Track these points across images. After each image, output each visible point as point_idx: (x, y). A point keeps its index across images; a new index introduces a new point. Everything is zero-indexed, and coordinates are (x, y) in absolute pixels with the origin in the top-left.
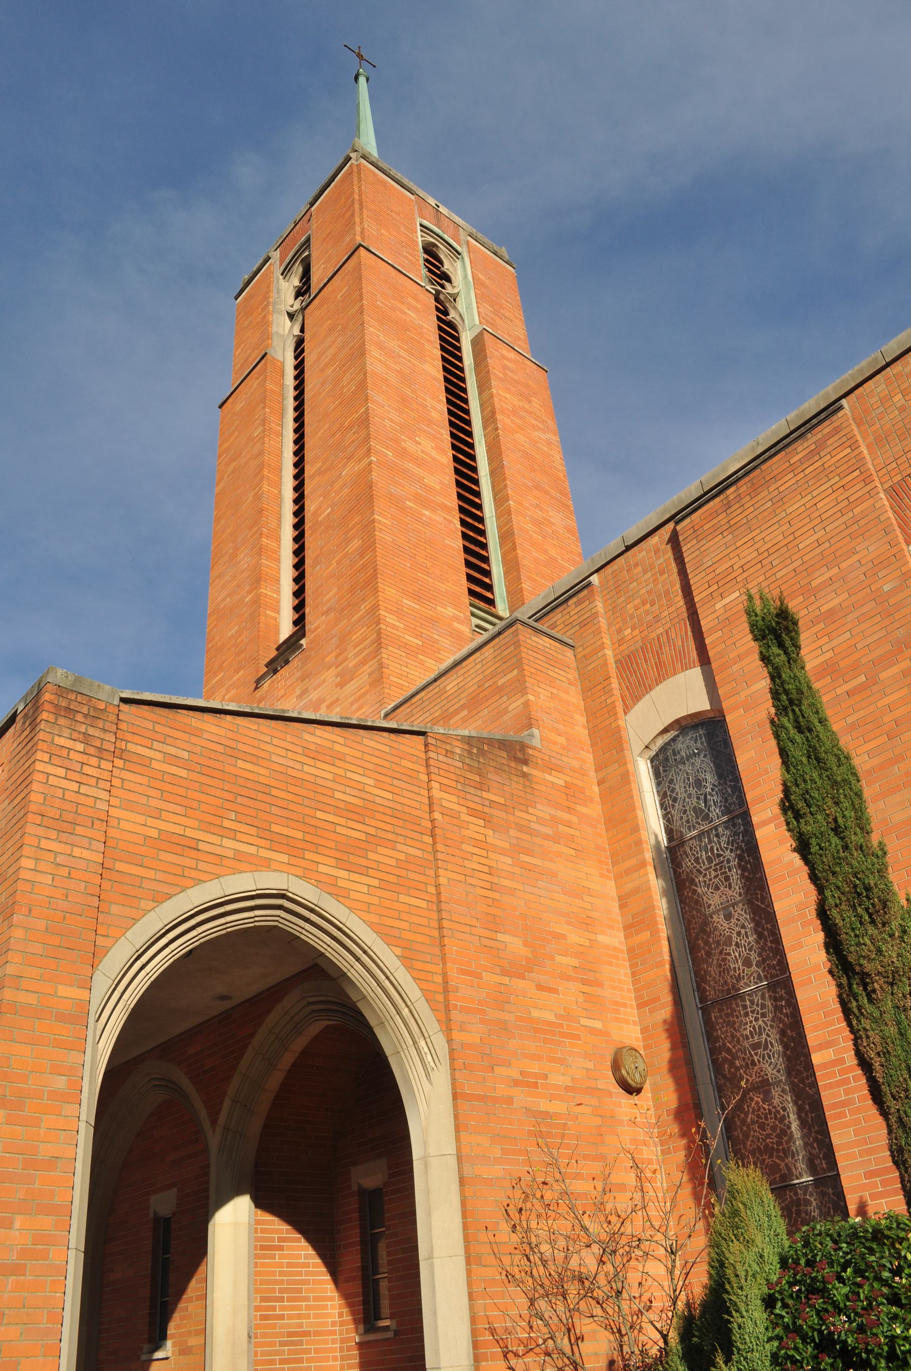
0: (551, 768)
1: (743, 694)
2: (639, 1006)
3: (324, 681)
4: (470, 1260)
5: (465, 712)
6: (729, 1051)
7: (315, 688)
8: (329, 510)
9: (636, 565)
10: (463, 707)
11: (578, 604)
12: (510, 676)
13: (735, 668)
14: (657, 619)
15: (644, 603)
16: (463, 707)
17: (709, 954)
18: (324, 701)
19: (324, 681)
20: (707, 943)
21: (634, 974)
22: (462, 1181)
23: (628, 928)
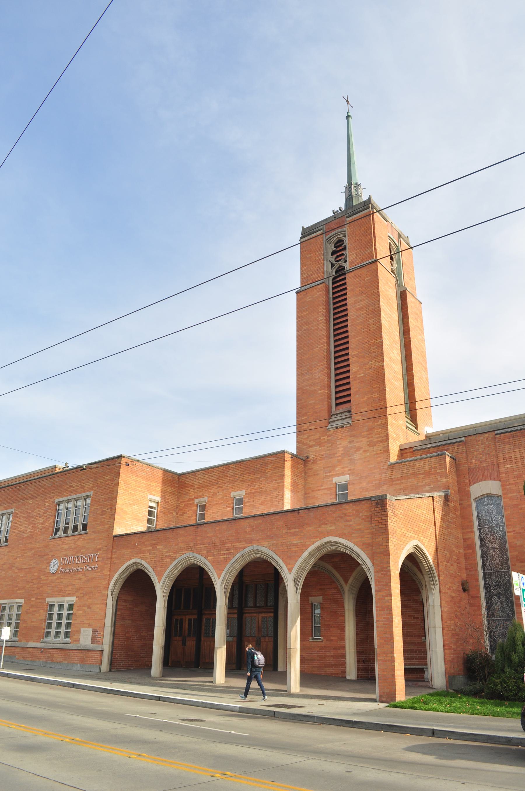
0: (452, 502)
1: (509, 495)
2: (466, 569)
3: (362, 441)
4: (443, 628)
5: (424, 476)
6: (490, 585)
7: (357, 442)
8: (363, 375)
9: (479, 441)
10: (422, 474)
11: (458, 446)
12: (442, 471)
13: (508, 487)
14: (484, 461)
15: (480, 454)
16: (422, 474)
17: (487, 559)
18: (362, 448)
19: (362, 441)
20: (487, 556)
21: (465, 560)
22: (442, 611)
23: (465, 548)
